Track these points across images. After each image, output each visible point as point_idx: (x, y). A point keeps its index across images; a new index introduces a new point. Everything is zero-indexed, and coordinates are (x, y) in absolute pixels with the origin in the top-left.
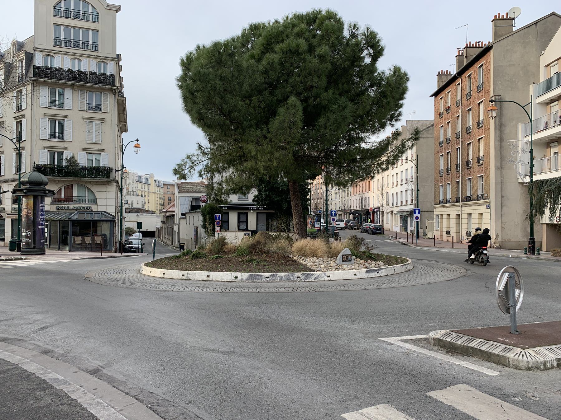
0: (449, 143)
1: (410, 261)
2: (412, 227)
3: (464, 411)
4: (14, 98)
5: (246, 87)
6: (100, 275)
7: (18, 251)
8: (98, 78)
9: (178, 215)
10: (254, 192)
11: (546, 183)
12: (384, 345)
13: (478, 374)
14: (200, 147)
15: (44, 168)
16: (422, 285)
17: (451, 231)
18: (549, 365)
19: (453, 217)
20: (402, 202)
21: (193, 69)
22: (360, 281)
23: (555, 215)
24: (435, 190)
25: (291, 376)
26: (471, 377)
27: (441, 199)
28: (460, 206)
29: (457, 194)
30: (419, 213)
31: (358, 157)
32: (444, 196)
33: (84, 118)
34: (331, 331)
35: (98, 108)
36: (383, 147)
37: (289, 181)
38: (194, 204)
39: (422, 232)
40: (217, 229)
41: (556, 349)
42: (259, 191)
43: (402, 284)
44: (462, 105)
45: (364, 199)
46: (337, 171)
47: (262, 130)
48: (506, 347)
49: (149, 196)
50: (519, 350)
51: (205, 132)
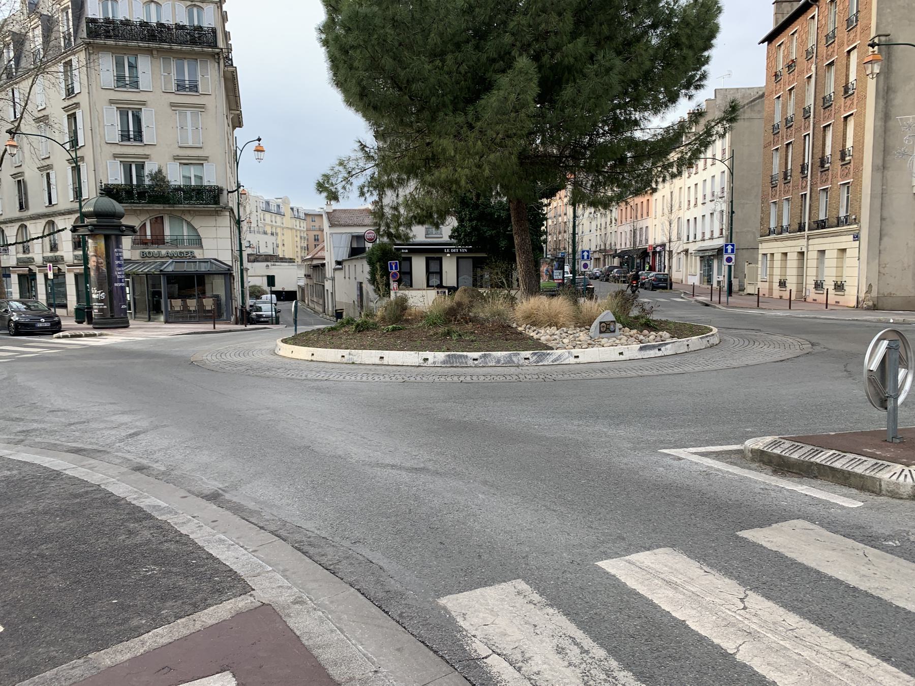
1: (715, 330)
2: (719, 276)
3: (799, 560)
4: (61, 74)
5: (434, 38)
6: (214, 358)
7: (89, 323)
8: (191, 36)
9: (330, 265)
10: (452, 222)
12: (669, 461)
13: (827, 504)
14: (363, 147)
15: (117, 190)
19: (793, 256)
21: (345, 8)
25: (516, 504)
26: (813, 509)
30: (733, 251)
31: (629, 155)
33: (172, 105)
34: (580, 439)
35: (194, 88)
36: (672, 138)
37: (509, 201)
38: (355, 245)
40: (394, 285)
42: (461, 220)
44: (816, 56)
45: (638, 229)
46: (593, 181)
47: (466, 114)
48: (876, 464)
49: (283, 234)
50: (898, 467)
51: (368, 119)
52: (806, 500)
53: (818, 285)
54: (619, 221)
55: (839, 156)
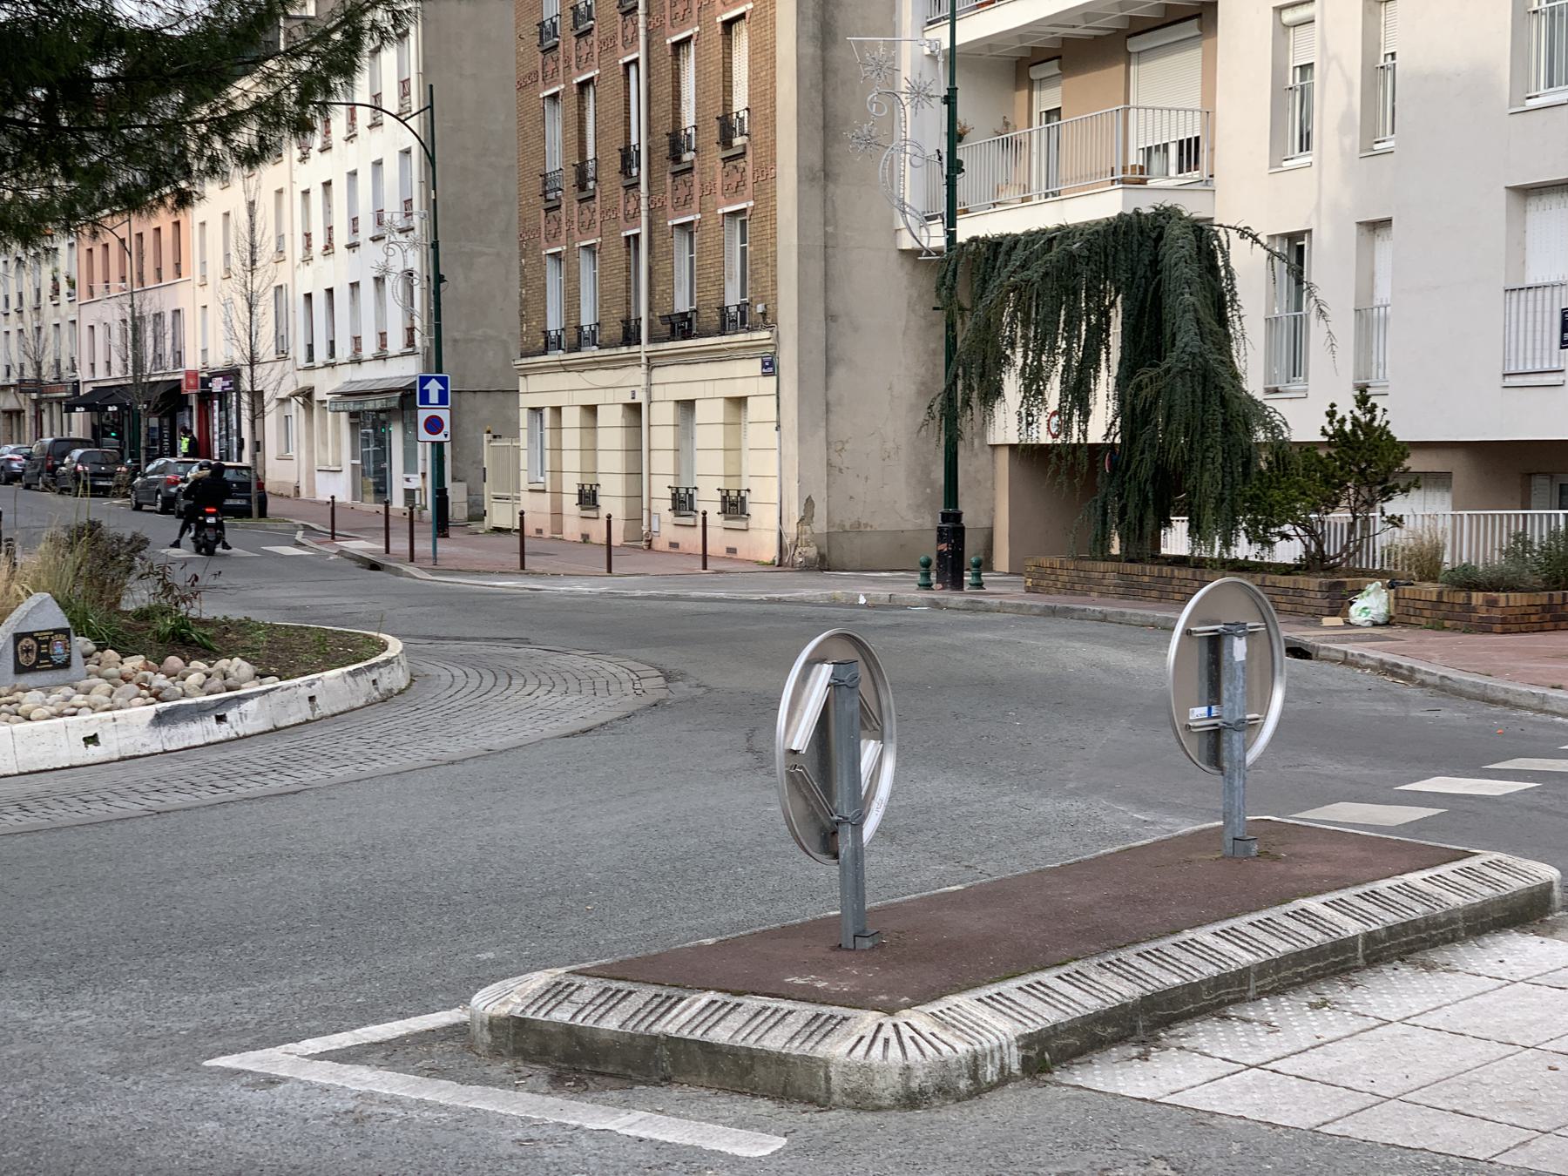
0: (589, 32)
1: (395, 646)
11: (1008, 253)
12: (236, 1093)
16: (453, 763)
17: (600, 492)
18: (990, 1072)
19: (612, 416)
20: (357, 340)
22: (120, 773)
23: (1044, 401)
24: (524, 282)
27: (554, 324)
28: (644, 360)
29: (628, 302)
30: (443, 398)
31: (98, 71)
32: (568, 312)
39: (465, 497)
41: (1020, 997)
43: (350, 770)
48: (817, 1016)
50: (870, 1019)
52: (639, 1155)
53: (682, 502)
54: (82, 286)
55: (715, 132)
